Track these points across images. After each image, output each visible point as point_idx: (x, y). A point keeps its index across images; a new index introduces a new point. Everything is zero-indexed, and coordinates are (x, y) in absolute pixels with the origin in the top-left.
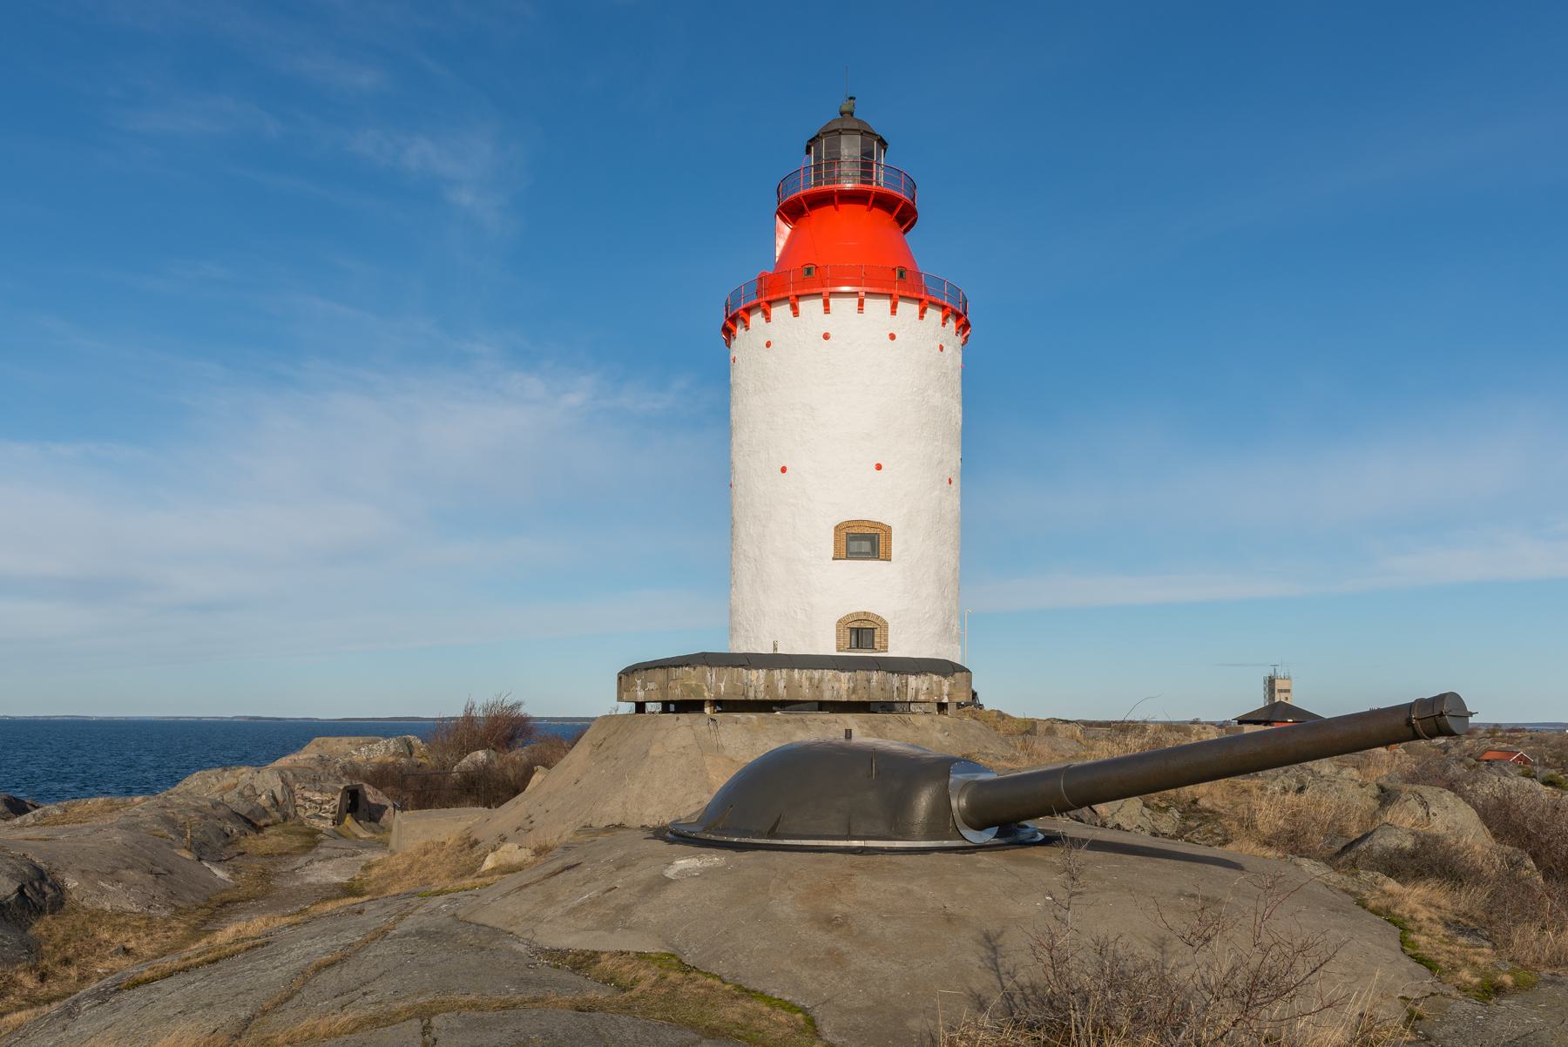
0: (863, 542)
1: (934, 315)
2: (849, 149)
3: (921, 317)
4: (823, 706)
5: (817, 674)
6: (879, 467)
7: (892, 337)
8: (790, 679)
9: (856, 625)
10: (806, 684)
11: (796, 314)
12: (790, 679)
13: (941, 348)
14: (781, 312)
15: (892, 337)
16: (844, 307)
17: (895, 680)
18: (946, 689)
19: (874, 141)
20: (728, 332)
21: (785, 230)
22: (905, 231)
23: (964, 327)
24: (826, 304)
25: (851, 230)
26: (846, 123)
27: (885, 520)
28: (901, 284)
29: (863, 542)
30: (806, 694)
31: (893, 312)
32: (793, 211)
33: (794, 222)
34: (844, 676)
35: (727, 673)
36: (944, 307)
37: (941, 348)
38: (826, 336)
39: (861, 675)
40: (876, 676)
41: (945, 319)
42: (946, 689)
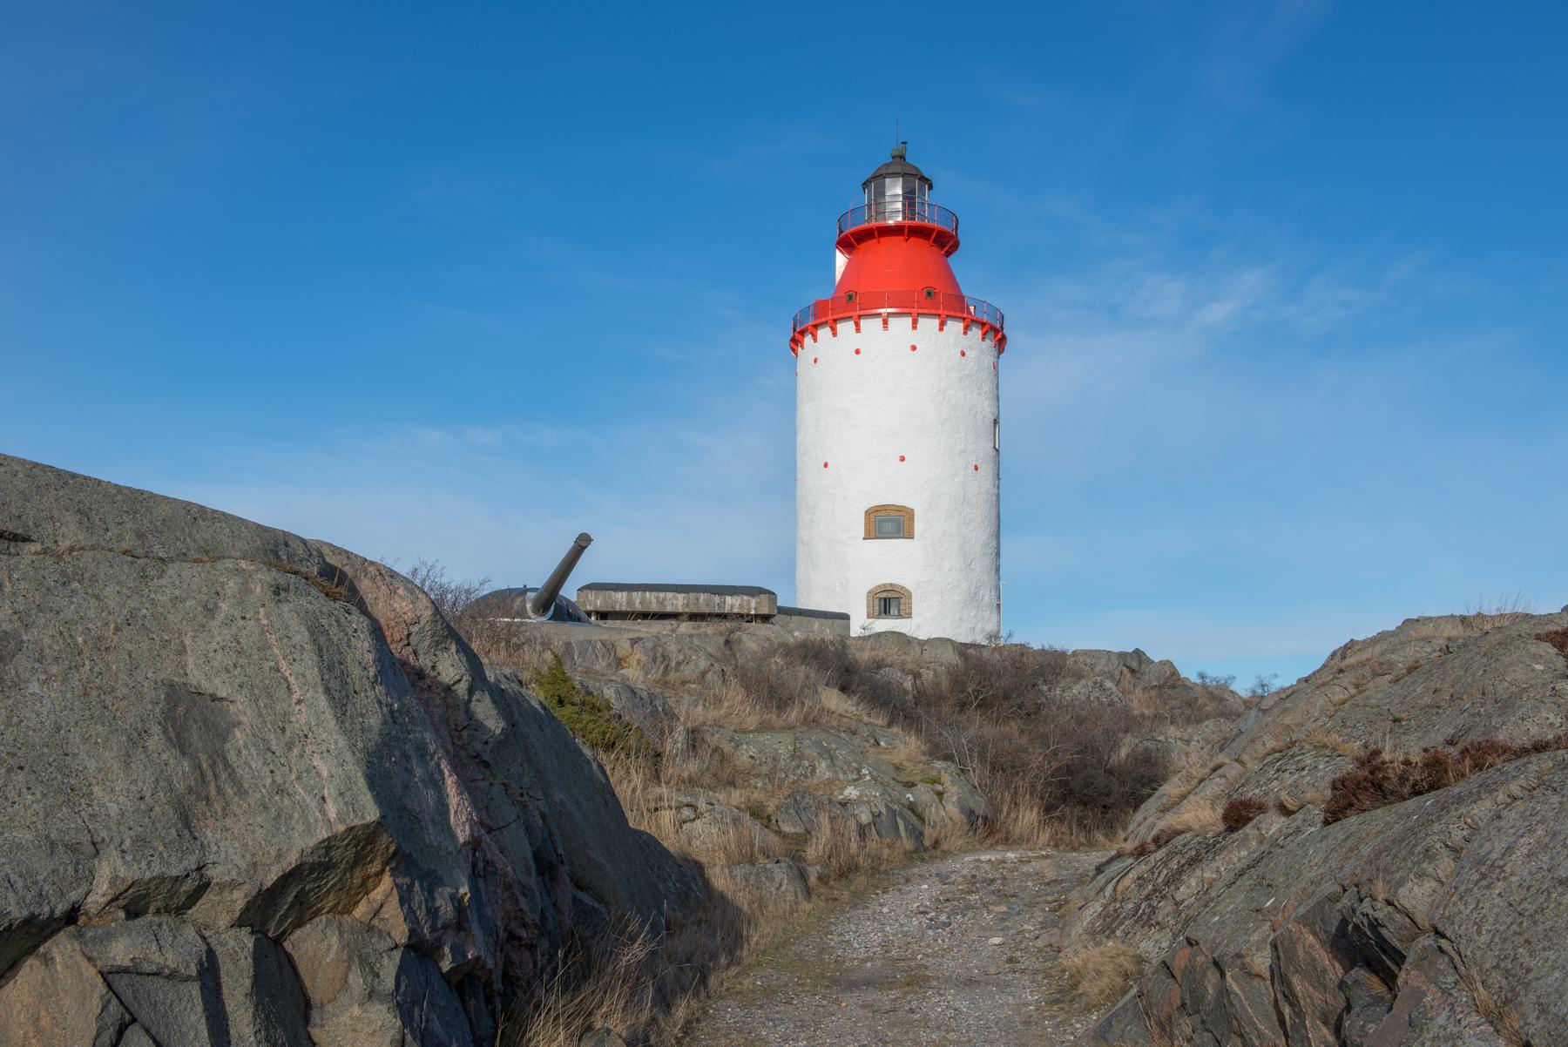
0: (889, 522)
1: (976, 332)
2: (895, 189)
3: (941, 329)
4: (645, 616)
5: (662, 595)
6: (903, 459)
7: (914, 348)
8: (643, 598)
9: (884, 595)
10: (654, 601)
11: (835, 334)
12: (643, 598)
13: (963, 354)
14: (824, 333)
15: (914, 348)
16: (871, 326)
17: (717, 599)
18: (753, 605)
19: (917, 182)
20: (796, 342)
21: (841, 260)
22: (948, 254)
23: (1001, 343)
24: (885, 322)
25: (893, 258)
26: (900, 166)
27: (909, 504)
28: (943, 302)
29: (889, 522)
30: (654, 608)
31: (914, 327)
32: (846, 244)
33: (850, 253)
34: (681, 596)
35: (601, 594)
36: (983, 324)
37: (963, 354)
38: (858, 352)
39: (692, 595)
40: (702, 596)
41: (966, 329)
42: (753, 605)
